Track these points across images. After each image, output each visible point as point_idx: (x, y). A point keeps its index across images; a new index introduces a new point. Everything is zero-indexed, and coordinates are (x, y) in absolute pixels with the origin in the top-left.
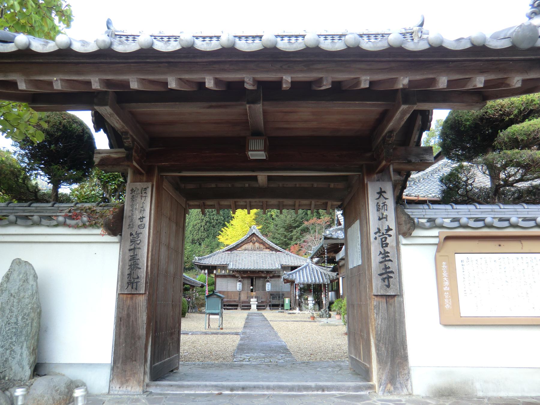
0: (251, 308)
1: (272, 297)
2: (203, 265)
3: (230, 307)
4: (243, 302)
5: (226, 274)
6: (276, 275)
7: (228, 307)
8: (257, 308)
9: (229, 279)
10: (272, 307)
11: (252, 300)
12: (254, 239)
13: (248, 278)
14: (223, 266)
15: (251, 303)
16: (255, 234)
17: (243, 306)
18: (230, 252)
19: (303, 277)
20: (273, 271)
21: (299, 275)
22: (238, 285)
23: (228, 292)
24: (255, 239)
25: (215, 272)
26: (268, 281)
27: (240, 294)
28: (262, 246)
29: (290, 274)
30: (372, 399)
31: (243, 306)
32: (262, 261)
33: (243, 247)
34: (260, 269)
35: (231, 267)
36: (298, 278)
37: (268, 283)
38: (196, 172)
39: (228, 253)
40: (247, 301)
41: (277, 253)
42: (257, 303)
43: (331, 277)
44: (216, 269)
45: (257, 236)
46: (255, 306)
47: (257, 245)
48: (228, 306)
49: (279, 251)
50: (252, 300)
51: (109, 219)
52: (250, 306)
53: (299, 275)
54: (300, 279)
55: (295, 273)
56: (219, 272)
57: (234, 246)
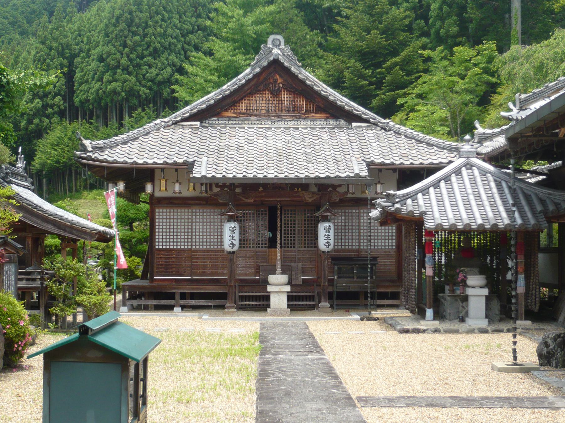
0: (269, 306)
1: (336, 268)
2: (108, 168)
3: (202, 303)
4: (244, 284)
5: (185, 194)
6: (350, 196)
7: (193, 302)
8: (289, 306)
9: (197, 211)
10: (340, 302)
11: (272, 278)
12: (275, 81)
13: (258, 206)
14: (176, 170)
15: (269, 289)
16: (282, 65)
17: (242, 298)
18: (198, 123)
19: (454, 205)
20: (340, 186)
21: (440, 201)
22: (227, 233)
23: (191, 253)
24: (280, 80)
25: (149, 188)
26: (325, 219)
27: (231, 260)
28: (303, 103)
29: (407, 196)
30: (179, 64)
31: (242, 298)
32: (305, 153)
33: (242, 106)
34: (297, 178)
35: (200, 171)
36: (436, 209)
37: (327, 224)
38: (348, 301)
39: (192, 127)
40: (257, 281)
41: (354, 124)
42: (288, 288)
43: (551, 208)
44: (152, 181)
45: (287, 71)
46: (284, 298)
47: (286, 98)
48: (193, 296)
49: (359, 119)
50: (272, 278)
51: (435, 188)
52: (267, 298)
53: (440, 201)
54: (443, 212)
55: (425, 191)
56: (163, 189)
57: (212, 102)
